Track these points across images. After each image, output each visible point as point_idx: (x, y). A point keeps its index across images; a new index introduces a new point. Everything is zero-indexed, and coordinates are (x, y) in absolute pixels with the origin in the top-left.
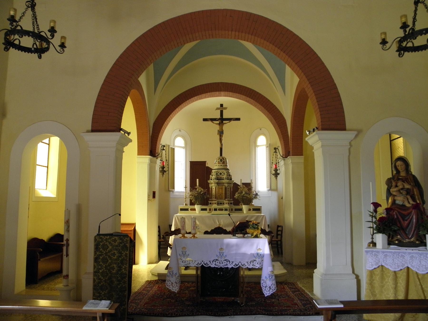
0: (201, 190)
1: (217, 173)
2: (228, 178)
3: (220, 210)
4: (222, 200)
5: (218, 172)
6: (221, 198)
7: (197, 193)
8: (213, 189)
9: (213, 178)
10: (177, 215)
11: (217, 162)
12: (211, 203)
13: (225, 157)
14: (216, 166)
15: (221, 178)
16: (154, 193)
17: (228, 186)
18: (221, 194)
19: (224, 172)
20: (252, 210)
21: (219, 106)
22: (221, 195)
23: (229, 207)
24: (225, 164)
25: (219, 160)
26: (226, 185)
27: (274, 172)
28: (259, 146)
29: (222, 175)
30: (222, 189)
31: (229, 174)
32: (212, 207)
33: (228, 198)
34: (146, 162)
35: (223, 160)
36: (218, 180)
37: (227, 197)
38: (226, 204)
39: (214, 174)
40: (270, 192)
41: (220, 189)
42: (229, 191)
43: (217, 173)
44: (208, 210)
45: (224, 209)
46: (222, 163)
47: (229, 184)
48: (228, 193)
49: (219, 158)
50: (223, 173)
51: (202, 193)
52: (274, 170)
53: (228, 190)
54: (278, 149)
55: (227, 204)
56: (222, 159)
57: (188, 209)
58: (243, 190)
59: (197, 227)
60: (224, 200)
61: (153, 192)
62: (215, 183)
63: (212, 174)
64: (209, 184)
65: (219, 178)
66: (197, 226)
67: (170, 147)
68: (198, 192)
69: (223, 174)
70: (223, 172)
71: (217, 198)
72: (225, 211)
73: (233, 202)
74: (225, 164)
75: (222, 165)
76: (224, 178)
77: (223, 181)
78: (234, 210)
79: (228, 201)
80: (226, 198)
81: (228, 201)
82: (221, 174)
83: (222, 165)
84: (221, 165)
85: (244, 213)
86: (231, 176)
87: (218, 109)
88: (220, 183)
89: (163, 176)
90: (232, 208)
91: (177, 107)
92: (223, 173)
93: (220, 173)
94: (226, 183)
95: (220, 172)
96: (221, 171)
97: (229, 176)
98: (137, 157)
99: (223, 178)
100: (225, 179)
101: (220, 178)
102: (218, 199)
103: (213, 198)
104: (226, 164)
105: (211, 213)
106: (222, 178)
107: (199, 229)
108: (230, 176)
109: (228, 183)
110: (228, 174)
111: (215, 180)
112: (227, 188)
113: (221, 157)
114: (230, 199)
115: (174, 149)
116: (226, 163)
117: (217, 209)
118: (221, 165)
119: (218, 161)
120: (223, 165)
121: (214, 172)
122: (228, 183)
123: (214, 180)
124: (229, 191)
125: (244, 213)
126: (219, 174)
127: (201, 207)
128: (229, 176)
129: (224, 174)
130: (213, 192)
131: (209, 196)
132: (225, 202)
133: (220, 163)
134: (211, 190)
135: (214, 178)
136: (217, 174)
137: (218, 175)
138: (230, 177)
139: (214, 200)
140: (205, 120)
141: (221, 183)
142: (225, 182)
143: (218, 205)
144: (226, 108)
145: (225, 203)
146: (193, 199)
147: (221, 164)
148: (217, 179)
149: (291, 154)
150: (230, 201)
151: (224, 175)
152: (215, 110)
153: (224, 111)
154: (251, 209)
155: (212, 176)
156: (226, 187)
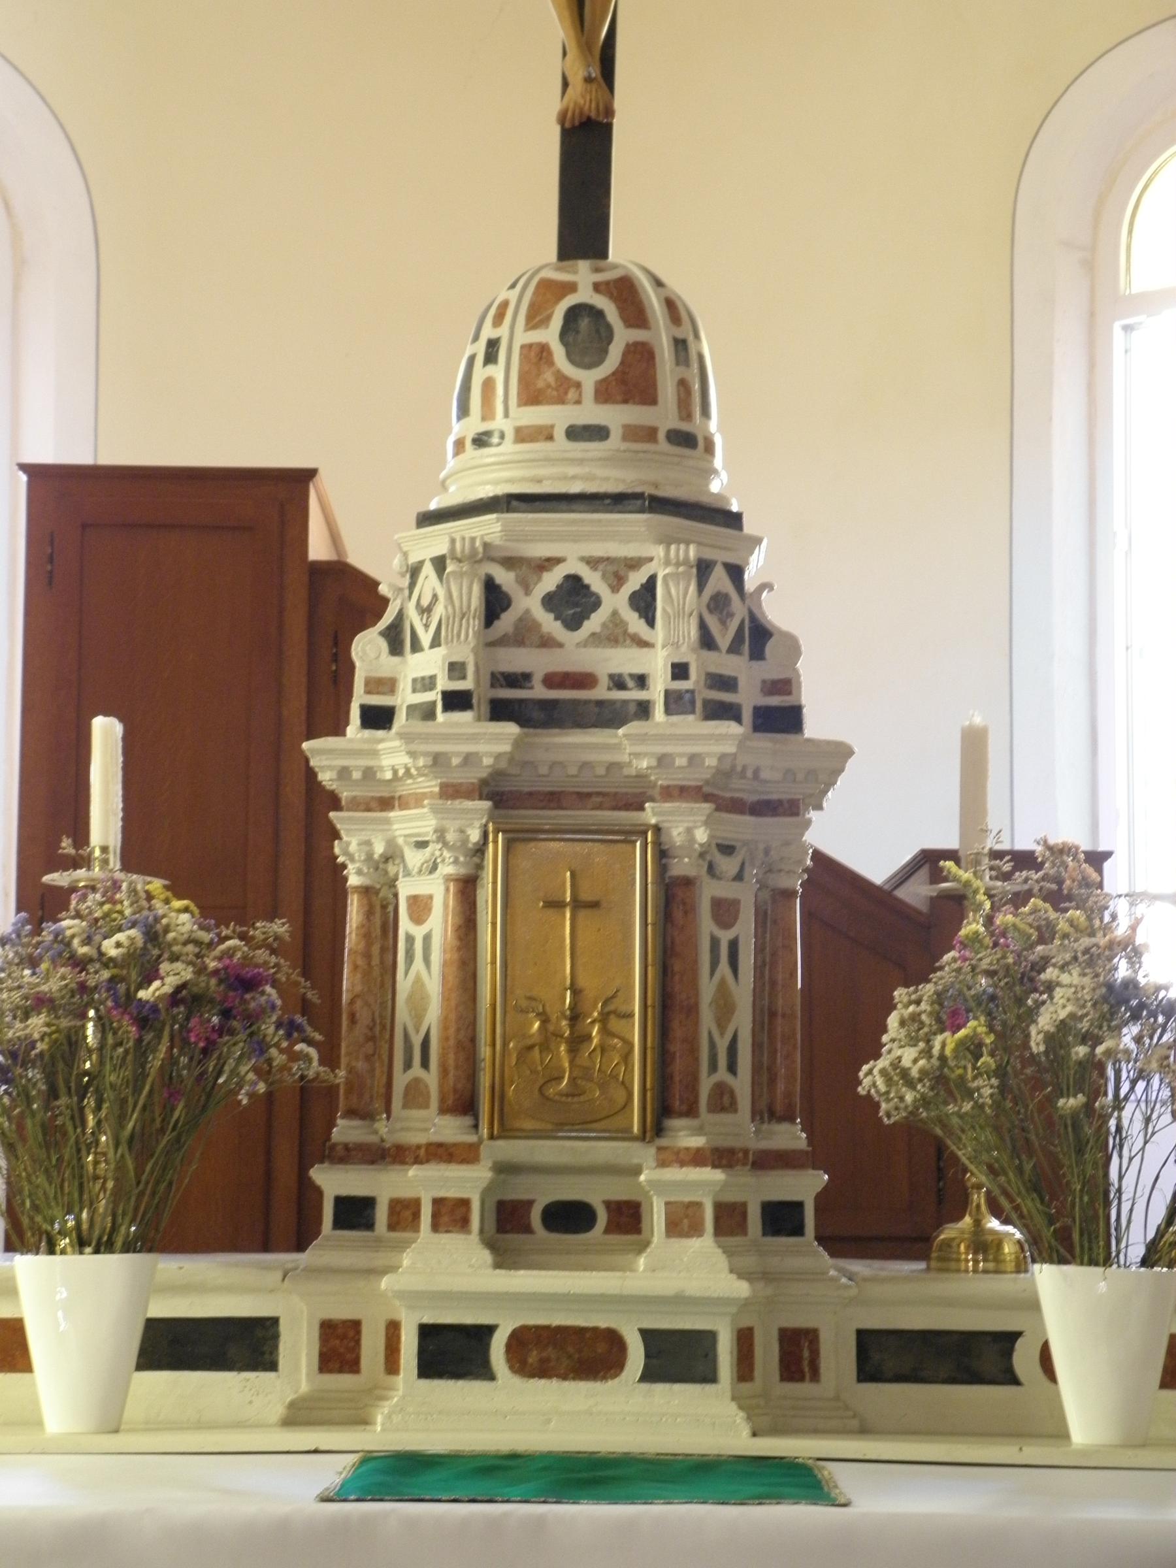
0: (153, 934)
1: (492, 589)
3: (543, 1371)
5: (510, 562)
6: (575, 1091)
7: (52, 986)
8: (420, 907)
9: (405, 698)
11: (491, 357)
12: (368, 1203)
13: (659, 283)
14: (481, 441)
15: (584, 680)
17: (727, 849)
18: (575, 1017)
19: (635, 564)
22: (578, 1041)
23: (742, 1289)
24: (665, 416)
25: (551, 334)
28: (1147, 302)
29: (594, 623)
30: (595, 905)
31: (739, 611)
32: (385, 1283)
33: (723, 1100)
35: (623, 336)
36: (511, 729)
37: (706, 1085)
39: (425, 611)
41: (555, 905)
42: (747, 959)
43: (505, 578)
45: (646, 1334)
46: (604, 393)
47: (736, 806)
48: (725, 1008)
49: (550, 291)
50: (617, 581)
51: (175, 997)
55: (695, 1230)
56: (597, 314)
58: (1046, 933)
60: (644, 1154)
62: (450, 792)
63: (388, 618)
64: (334, 802)
65: (539, 692)
68: (80, 964)
71: (499, 1096)
72: (650, 1375)
73: (823, 1200)
74: (665, 416)
75: (598, 433)
76: (641, 681)
79: (721, 1157)
80: (691, 1111)
81: (716, 1176)
83: (598, 433)
84: (576, 433)
86: (793, 647)
88: (553, 799)
92: (617, 581)
93: (551, 581)
94: (682, 792)
95: (551, 562)
97: (734, 648)
99: (618, 683)
100: (659, 713)
101: (553, 680)
102: (504, 1130)
103: (415, 1095)
104: (687, 416)
105: (364, 1421)
106: (602, 692)
108: (757, 654)
110: (719, 604)
111: (466, 717)
112: (709, 891)
113: (583, 266)
114: (756, 1114)
116: (683, 385)
117: (483, 1333)
118: (576, 433)
119: (524, 337)
120: (614, 416)
121: (439, 563)
123: (441, 716)
124: (747, 959)
125: (1061, 1434)
126: (549, 601)
127: (146, 1288)
128: (734, 648)
129: (644, 601)
130: (404, 984)
131: (315, 1068)
133: (564, 391)
134: (366, 935)
135: (428, 683)
137: (525, 635)
138: (769, 669)
139: (433, 1136)
141: (583, 798)
142: (663, 761)
143: (504, 1259)
145: (657, 1217)
146: (918, 1092)
147: (590, 413)
148: (500, 711)
150: (767, 1161)
151: (651, 622)
152: (431, 930)
155: (396, 648)
156: (682, 866)
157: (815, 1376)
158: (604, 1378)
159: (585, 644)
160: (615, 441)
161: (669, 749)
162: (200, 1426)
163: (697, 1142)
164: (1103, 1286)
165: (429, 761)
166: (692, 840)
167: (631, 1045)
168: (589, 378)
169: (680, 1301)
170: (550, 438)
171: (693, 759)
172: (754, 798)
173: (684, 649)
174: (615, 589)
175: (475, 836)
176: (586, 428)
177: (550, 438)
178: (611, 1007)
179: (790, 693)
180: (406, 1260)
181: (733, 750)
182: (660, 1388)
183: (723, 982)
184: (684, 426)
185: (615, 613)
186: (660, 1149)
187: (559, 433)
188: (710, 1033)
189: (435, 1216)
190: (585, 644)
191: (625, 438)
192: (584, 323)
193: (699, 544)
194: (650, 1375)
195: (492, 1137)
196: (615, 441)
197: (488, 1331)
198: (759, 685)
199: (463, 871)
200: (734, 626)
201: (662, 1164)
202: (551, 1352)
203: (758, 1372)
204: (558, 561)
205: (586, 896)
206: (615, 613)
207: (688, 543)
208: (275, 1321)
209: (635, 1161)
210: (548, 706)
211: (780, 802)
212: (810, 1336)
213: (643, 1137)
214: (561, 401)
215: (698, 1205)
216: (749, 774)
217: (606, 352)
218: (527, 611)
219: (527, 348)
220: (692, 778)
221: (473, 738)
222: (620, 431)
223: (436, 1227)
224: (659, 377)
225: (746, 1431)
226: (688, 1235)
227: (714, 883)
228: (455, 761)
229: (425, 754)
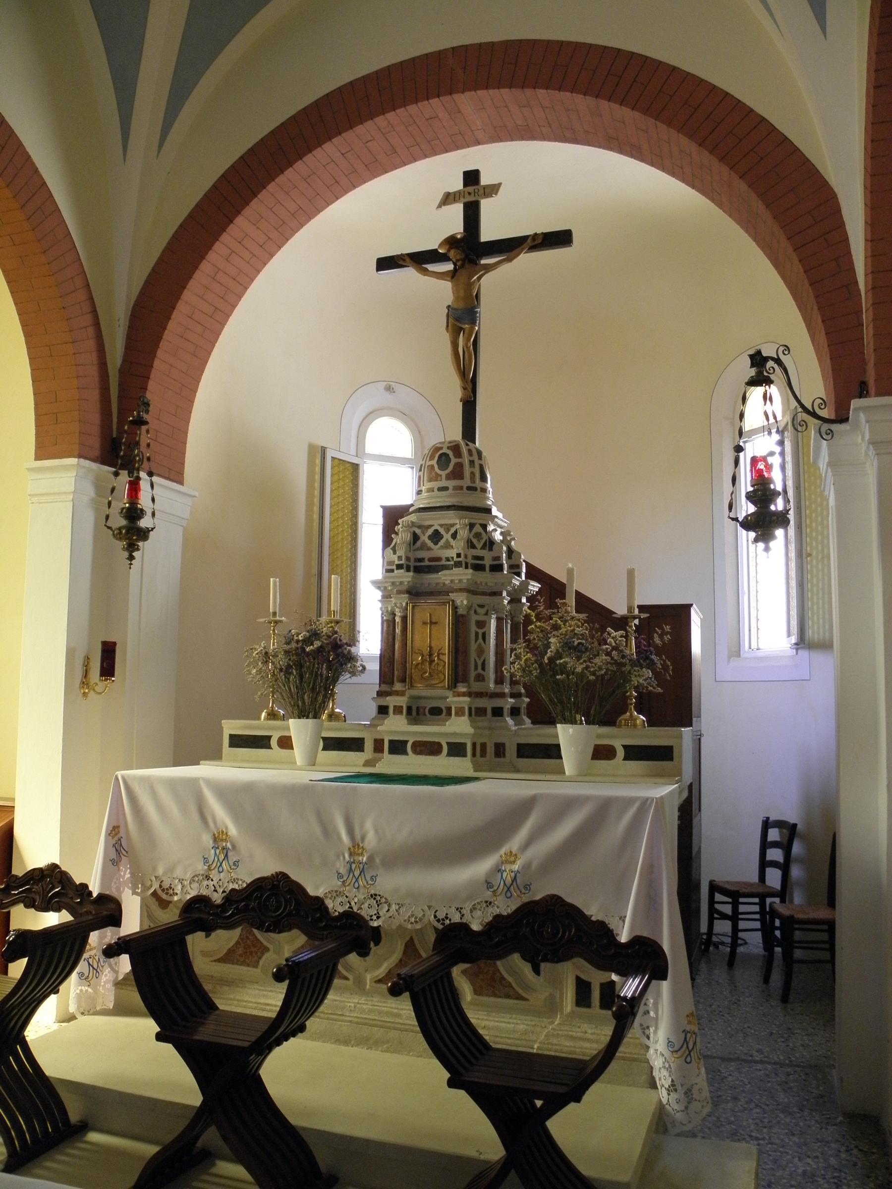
2: (481, 558)
4: (438, 692)
5: (419, 527)
10: (129, 776)
15: (438, 559)
16: (109, 651)
18: (431, 655)
19: (452, 525)
20: (621, 753)
21: (458, 184)
22: (431, 662)
25: (434, 462)
26: (462, 600)
27: (747, 508)
30: (436, 623)
31: (485, 537)
34: (65, 493)
35: (454, 461)
38: (460, 712)
40: (804, 654)
43: (418, 531)
44: (369, 745)
45: (448, 743)
46: (448, 477)
50: (448, 531)
52: (750, 497)
53: (481, 631)
54: (778, 361)
55: (463, 714)
57: (269, 738)
59: (230, 854)
60: (449, 693)
61: (104, 644)
65: (427, 563)
66: (229, 845)
67: (329, 454)
69: (447, 536)
70: (448, 527)
72: (449, 754)
75: (445, 489)
77: (445, 577)
78: (511, 751)
79: (470, 694)
81: (467, 699)
82: (436, 537)
83: (445, 489)
84: (441, 489)
85: (567, 773)
87: (452, 197)
89: (131, 558)
90: (499, 741)
91: (239, 212)
92: (448, 531)
93: (430, 532)
95: (430, 526)
96: (436, 521)
97: (483, 547)
98: (29, 470)
101: (430, 560)
106: (444, 562)
107: (236, 864)
108: (491, 549)
109: (471, 591)
111: (402, 571)
115: (355, 468)
117: (269, 738)
120: (451, 484)
122: (471, 591)
123: (396, 571)
126: (430, 537)
128: (483, 547)
129: (454, 536)
132: (455, 701)
133: (437, 477)
136: (416, 537)
137: (424, 547)
138: (494, 554)
140: (385, 264)
144: (492, 190)
147: (444, 483)
149: (872, 390)
152: (439, 206)
153: (486, 205)
154: (618, 745)
156: (461, 611)
157: (504, 756)
158: (437, 755)
159: (438, 549)
160: (450, 491)
161: (453, 578)
162: (345, 765)
163: (464, 690)
164: (571, 731)
165: (391, 584)
166: (463, 604)
167: (445, 663)
168: (443, 473)
169: (455, 734)
170: (433, 491)
171: (460, 581)
172: (490, 591)
173: (460, 549)
174: (447, 533)
175: (404, 604)
176: (443, 487)
177: (433, 491)
178: (440, 652)
179: (500, 560)
180: (386, 722)
181: (470, 577)
182: (452, 758)
183: (480, 644)
184: (473, 485)
185: (447, 540)
186: (454, 692)
187: (436, 490)
188: (475, 660)
189: (394, 710)
190: (438, 549)
191: (453, 490)
192: (443, 458)
193: (469, 518)
194: (626, 758)
195: (409, 689)
196: (450, 491)
197: (406, 742)
198: (491, 558)
199: (402, 614)
200: (483, 542)
201: (454, 696)
202: (422, 748)
203: (488, 755)
204: (432, 526)
205: (434, 620)
206: (447, 540)
207: (466, 518)
208: (364, 739)
209: (447, 695)
210: (429, 567)
211: (497, 592)
212: (503, 745)
213: (449, 688)
214: (437, 480)
215: (464, 708)
216: (483, 584)
217: (449, 465)
218: (424, 541)
219: (428, 466)
220: (463, 586)
221: (401, 577)
222: (452, 488)
223: (394, 713)
224: (465, 471)
225: (472, 770)
226: (460, 716)
227: (476, 616)
228: (398, 584)
229: (390, 582)
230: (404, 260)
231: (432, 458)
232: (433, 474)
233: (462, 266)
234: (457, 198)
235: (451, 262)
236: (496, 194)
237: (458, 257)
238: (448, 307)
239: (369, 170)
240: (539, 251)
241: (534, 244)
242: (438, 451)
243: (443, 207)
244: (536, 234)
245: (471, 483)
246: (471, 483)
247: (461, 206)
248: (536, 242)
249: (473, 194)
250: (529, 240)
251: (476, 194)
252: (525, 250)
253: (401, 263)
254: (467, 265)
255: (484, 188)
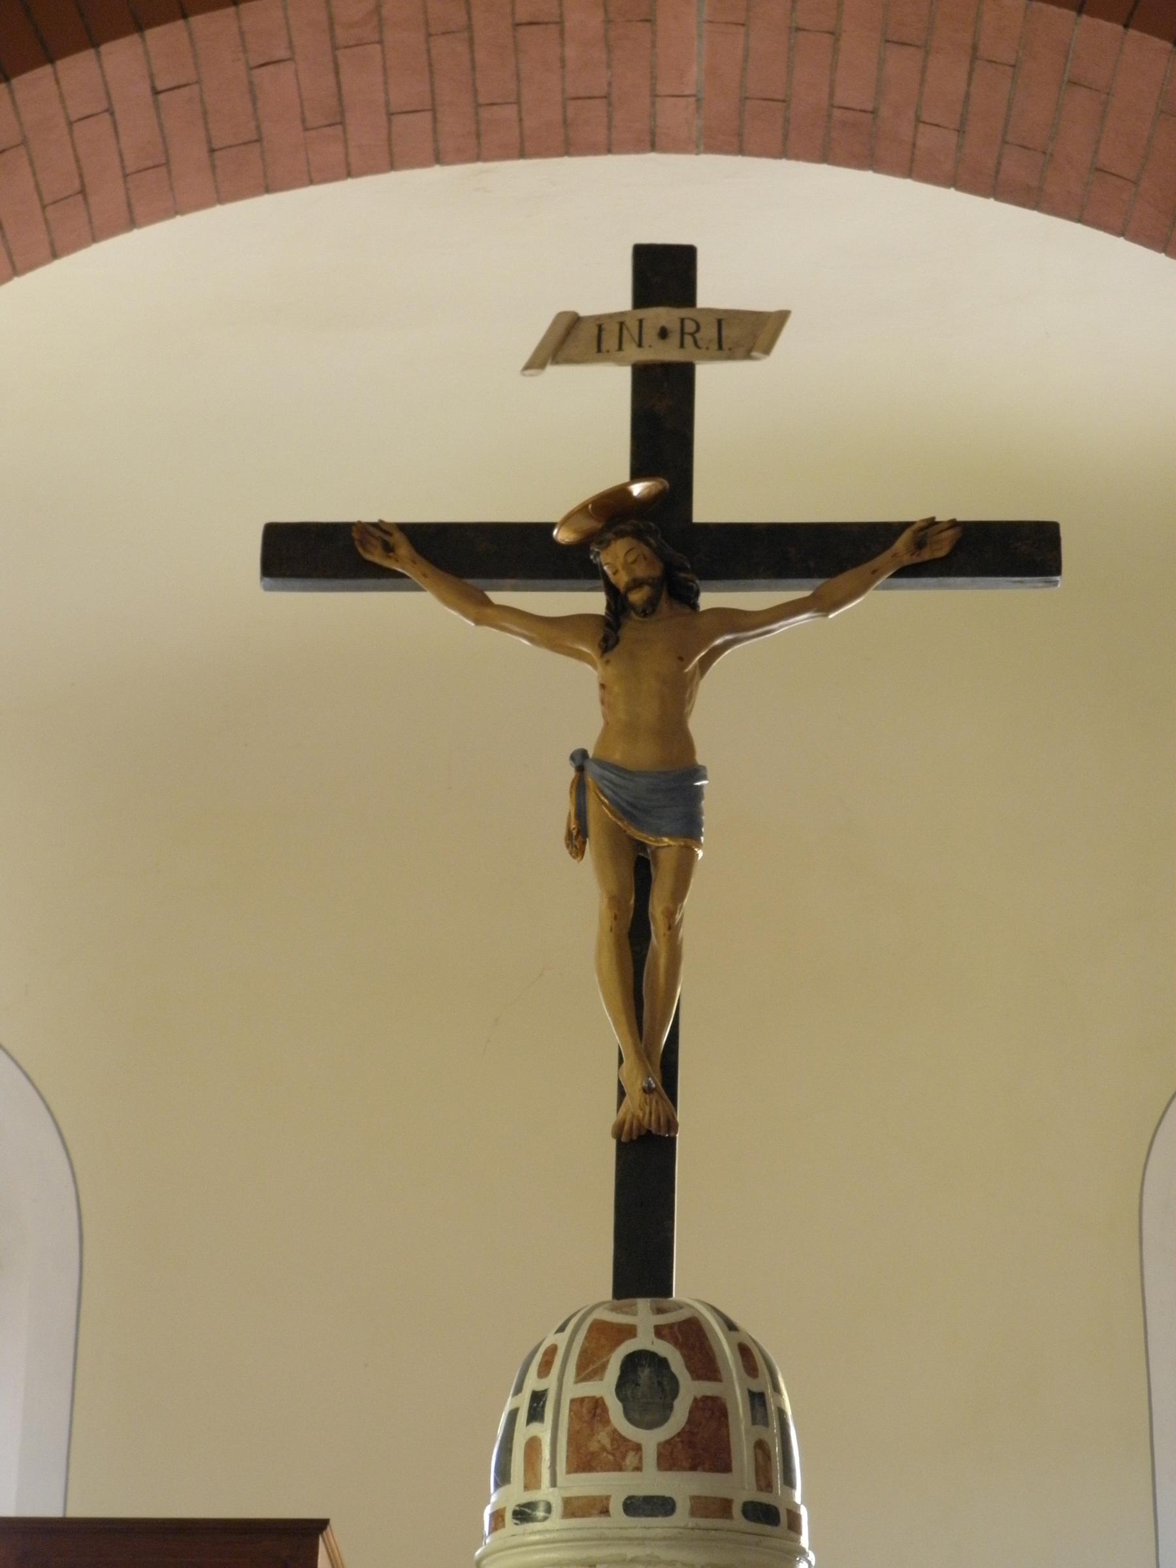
25: (605, 1387)
35: (690, 1389)
46: (669, 1458)
75: (661, 1506)
83: (661, 1506)
84: (635, 1506)
87: (588, 333)
152: (537, 363)
160: (682, 1516)
168: (650, 1440)
170: (605, 1512)
176: (648, 1500)
177: (605, 1512)
184: (764, 1498)
187: (616, 1506)
191: (693, 1513)
196: (682, 1516)
217: (671, 1408)
219: (577, 1402)
222: (688, 1504)
230: (388, 549)
231: (589, 1367)
232: (603, 1437)
233: (649, 609)
234: (610, 341)
235: (601, 583)
236: (767, 351)
237: (641, 571)
238: (580, 759)
239: (213, 167)
240: (603, 492)
241: (916, 559)
242: (618, 1342)
243: (552, 370)
244: (931, 523)
245: (760, 1489)
246: (760, 1489)
247: (624, 376)
248: (926, 555)
249: (674, 339)
250: (902, 543)
251: (688, 340)
252: (891, 573)
253: (376, 557)
254: (664, 605)
255: (720, 322)
